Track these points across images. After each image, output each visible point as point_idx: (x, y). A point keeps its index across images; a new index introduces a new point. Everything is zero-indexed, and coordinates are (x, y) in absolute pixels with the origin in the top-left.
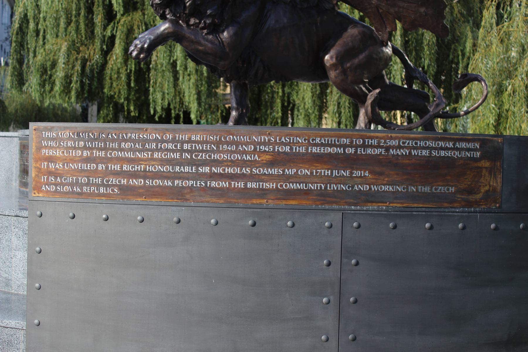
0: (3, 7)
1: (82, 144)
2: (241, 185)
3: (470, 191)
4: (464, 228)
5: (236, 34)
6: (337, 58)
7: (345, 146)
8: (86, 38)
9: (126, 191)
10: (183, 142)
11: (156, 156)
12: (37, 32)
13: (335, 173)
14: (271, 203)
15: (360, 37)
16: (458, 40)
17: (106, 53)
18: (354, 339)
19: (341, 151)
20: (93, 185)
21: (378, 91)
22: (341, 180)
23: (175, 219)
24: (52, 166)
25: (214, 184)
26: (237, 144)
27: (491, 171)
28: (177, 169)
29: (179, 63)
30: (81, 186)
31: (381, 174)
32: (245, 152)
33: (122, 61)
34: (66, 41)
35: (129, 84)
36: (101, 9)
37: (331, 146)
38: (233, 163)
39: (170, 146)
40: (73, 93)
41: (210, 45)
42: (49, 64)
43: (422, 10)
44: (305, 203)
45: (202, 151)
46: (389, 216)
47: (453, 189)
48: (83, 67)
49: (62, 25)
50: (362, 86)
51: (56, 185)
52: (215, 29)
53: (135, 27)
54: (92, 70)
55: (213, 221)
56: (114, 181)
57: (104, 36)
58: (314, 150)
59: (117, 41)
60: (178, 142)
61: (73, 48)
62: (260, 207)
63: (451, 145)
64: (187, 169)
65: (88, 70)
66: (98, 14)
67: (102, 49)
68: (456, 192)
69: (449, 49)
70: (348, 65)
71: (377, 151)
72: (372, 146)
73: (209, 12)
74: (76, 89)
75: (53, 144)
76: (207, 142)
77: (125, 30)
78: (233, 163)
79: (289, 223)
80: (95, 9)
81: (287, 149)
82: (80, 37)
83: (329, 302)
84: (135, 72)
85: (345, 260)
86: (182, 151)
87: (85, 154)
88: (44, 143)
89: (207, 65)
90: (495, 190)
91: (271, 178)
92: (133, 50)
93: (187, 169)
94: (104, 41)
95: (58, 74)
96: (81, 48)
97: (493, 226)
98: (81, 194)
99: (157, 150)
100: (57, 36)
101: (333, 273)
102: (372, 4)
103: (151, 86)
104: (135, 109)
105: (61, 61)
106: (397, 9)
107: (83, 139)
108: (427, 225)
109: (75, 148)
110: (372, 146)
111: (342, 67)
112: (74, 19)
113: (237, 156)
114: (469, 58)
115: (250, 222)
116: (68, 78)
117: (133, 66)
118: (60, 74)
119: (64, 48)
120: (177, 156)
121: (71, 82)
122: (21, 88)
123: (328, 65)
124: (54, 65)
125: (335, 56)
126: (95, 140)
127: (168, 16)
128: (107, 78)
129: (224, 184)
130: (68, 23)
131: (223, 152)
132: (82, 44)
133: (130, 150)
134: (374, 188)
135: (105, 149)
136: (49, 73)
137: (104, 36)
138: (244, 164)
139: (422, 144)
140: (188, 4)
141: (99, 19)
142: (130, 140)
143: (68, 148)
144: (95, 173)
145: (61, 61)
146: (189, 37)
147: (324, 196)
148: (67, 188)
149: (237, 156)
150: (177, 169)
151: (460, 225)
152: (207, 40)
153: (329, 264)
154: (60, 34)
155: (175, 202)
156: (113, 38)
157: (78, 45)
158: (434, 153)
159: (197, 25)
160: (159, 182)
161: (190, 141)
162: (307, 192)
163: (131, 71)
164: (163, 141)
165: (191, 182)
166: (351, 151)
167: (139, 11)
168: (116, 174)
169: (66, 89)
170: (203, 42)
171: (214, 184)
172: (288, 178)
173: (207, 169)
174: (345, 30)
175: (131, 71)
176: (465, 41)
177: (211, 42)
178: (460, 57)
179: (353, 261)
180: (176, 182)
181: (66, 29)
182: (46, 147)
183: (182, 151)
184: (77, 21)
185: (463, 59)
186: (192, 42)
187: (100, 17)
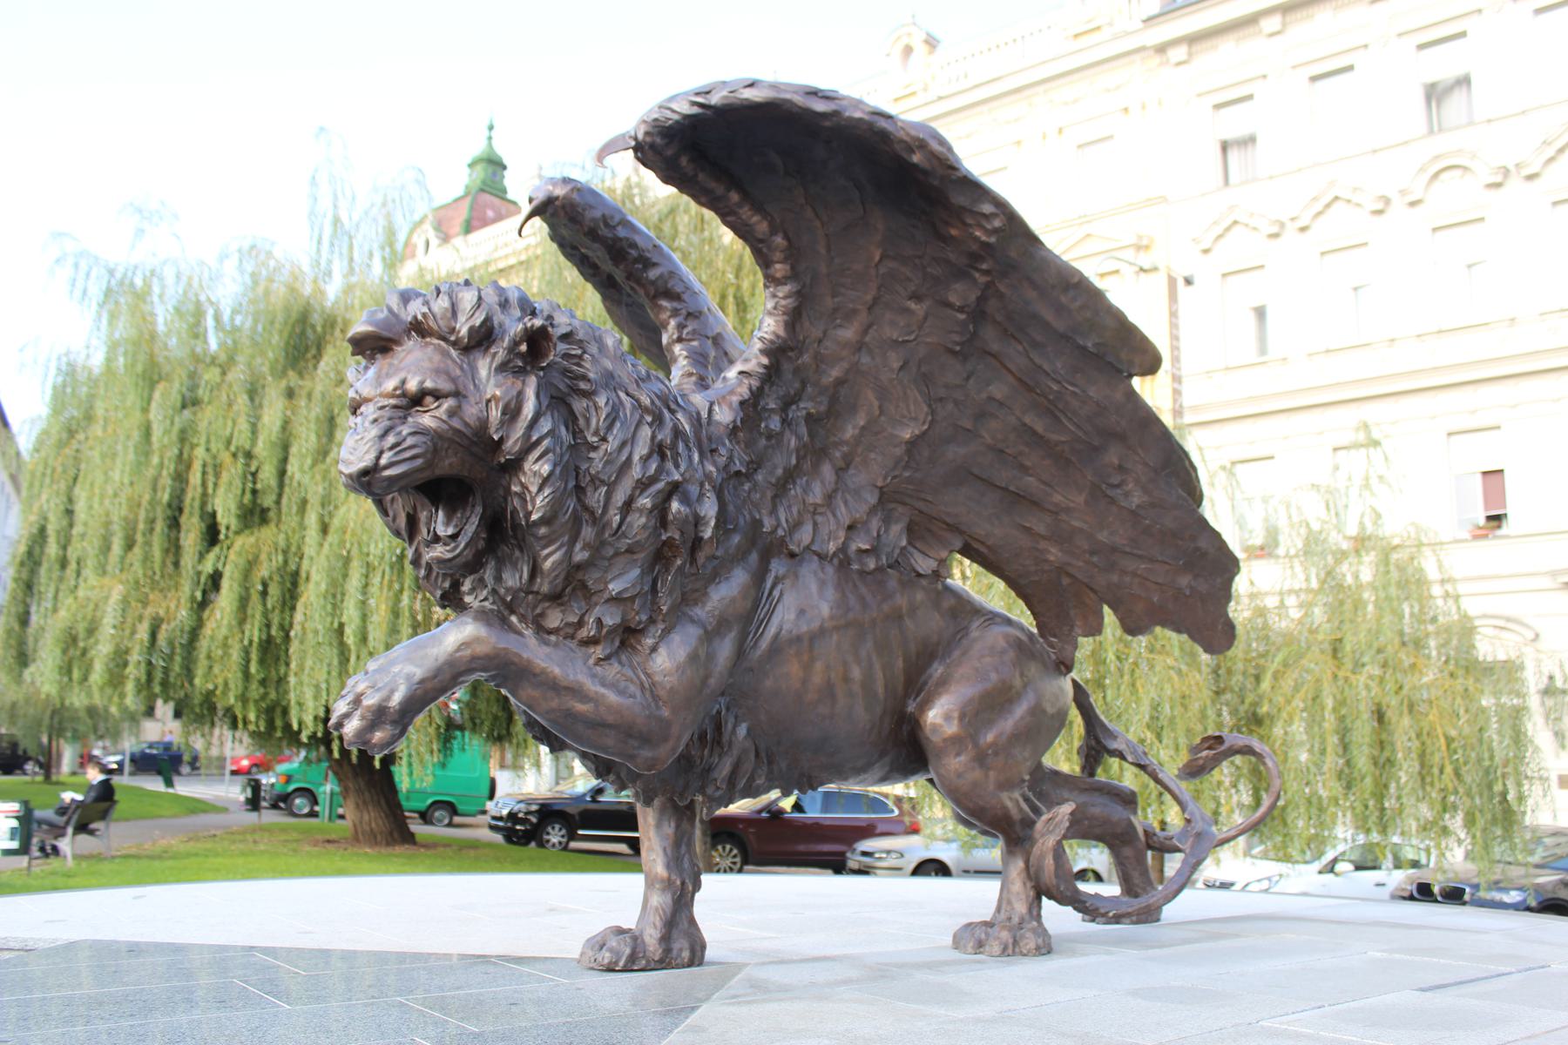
0: (8, 508)
6: (962, 717)
8: (162, 576)
12: (63, 563)
29: (348, 631)
34: (121, 582)
36: (195, 520)
40: (130, 687)
42: (81, 628)
48: (153, 635)
53: (263, 557)
54: (171, 643)
59: (225, 584)
61: (137, 596)
66: (188, 531)
67: (193, 599)
74: (138, 680)
77: (242, 561)
80: (183, 520)
89: (584, 757)
92: (347, 716)
95: (100, 647)
96: (151, 597)
100: (104, 573)
102: (1046, 561)
103: (292, 674)
104: (258, 717)
106: (1115, 578)
111: (976, 745)
112: (139, 538)
116: (120, 659)
117: (256, 633)
118: (102, 650)
119: (116, 596)
121: (126, 664)
122: (20, 675)
124: (91, 631)
125: (956, 715)
127: (468, 599)
128: (202, 656)
130: (129, 545)
136: (81, 644)
140: (548, 564)
141: (191, 536)
145: (107, 629)
146: (544, 671)
154: (109, 568)
156: (216, 579)
159: (570, 631)
163: (251, 642)
167: (272, 525)
169: (115, 679)
175: (251, 642)
181: (123, 559)
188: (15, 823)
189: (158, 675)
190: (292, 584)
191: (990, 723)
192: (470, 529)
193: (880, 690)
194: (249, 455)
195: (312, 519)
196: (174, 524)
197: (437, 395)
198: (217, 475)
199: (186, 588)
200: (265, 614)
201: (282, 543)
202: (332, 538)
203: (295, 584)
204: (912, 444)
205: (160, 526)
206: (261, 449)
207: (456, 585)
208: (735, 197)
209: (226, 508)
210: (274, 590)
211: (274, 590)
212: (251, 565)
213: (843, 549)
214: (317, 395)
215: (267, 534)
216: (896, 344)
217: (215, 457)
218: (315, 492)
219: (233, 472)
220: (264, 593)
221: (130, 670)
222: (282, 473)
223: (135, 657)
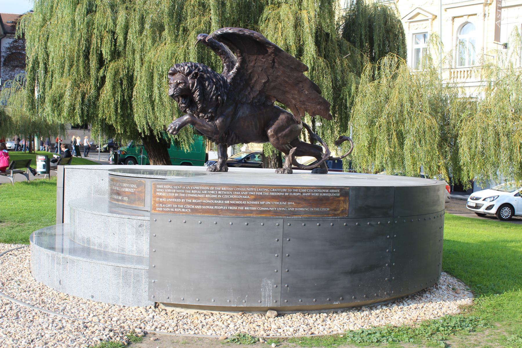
1: (174, 191)
2: (242, 208)
3: (336, 210)
4: (333, 225)
5: (223, 121)
7: (284, 192)
8: (84, 77)
9: (194, 211)
10: (218, 191)
11: (207, 196)
13: (280, 203)
14: (255, 216)
15: (286, 120)
16: (345, 84)
17: (99, 88)
18: (288, 271)
19: (283, 194)
20: (179, 208)
21: (295, 148)
22: (283, 206)
23: (215, 222)
24: (161, 200)
25: (231, 208)
26: (241, 191)
27: (344, 201)
28: (216, 202)
30: (174, 208)
31: (299, 203)
32: (244, 195)
33: (111, 94)
35: (116, 110)
36: (95, 56)
37: (279, 192)
38: (239, 199)
39: (213, 192)
41: (210, 127)
43: (318, 107)
44: (268, 216)
45: (226, 194)
46: (302, 221)
47: (328, 209)
49: (67, 67)
50: (287, 146)
51: (163, 208)
52: (212, 119)
53: (120, 70)
54: (89, 101)
55: (230, 223)
56: (189, 206)
57: (97, 77)
58: (272, 194)
59: (107, 80)
60: (216, 190)
61: (76, 84)
62: (250, 217)
63: (327, 191)
64: (220, 202)
65: (86, 100)
67: (96, 86)
68: (330, 210)
69: (340, 91)
70: (280, 135)
71: (298, 194)
72: (295, 192)
73: (210, 111)
75: (161, 190)
76: (228, 191)
77: (113, 72)
78: (239, 199)
79: (262, 224)
80: (90, 57)
81: (261, 193)
82: (79, 76)
83: (278, 256)
84: (120, 102)
85: (284, 239)
86: (218, 194)
87: (176, 195)
88: (158, 190)
90: (345, 209)
91: (254, 205)
93: (220, 202)
94: (98, 79)
97: (345, 224)
98: (174, 212)
99: (207, 194)
101: (279, 244)
105: (67, 94)
107: (175, 189)
108: (318, 224)
109: (171, 192)
110: (295, 192)
113: (241, 197)
114: (353, 97)
115: (246, 224)
116: (72, 108)
117: (119, 98)
118: (67, 103)
119: (69, 85)
120: (215, 196)
123: (269, 135)
124: (61, 96)
126: (180, 189)
129: (235, 208)
130: (71, 66)
131: (235, 195)
132: (81, 82)
133: (196, 193)
134: (296, 209)
135: (185, 193)
137: (97, 77)
138: (243, 199)
139: (316, 191)
142: (196, 189)
143: (168, 192)
144: (180, 203)
145: (67, 94)
147: (276, 213)
148: (168, 209)
149: (241, 197)
150: (216, 202)
151: (331, 224)
152: (208, 124)
153: (278, 240)
155: (214, 215)
156: (104, 78)
157: (79, 82)
158: (321, 195)
160: (208, 207)
161: (221, 190)
162: (269, 211)
163: (117, 101)
164: (210, 190)
165: (221, 207)
166: (287, 194)
168: (190, 203)
170: (206, 125)
171: (231, 208)
172: (261, 206)
173: (228, 202)
174: (279, 116)
175: (117, 101)
176: (351, 86)
177: (210, 125)
178: (348, 96)
179: (288, 239)
180: (215, 207)
181: (69, 70)
182: (158, 192)
183: (218, 194)
184: (78, 65)
185: (350, 97)
186: (201, 126)
187: (94, 62)
188: (44, 163)
189: (85, 113)
190: (131, 79)
191: (280, 132)
192: (188, 102)
193: (258, 127)
194: (114, 33)
195: (137, 56)
196: (87, 57)
197: (182, 83)
198: (102, 40)
199: (93, 82)
200: (123, 91)
201: (127, 65)
202: (146, 65)
203: (132, 81)
204: (265, 83)
205: (82, 59)
206: (118, 30)
207: (186, 110)
208: (230, 44)
209: (106, 51)
210: (125, 82)
211: (125, 82)
212: (117, 73)
213: (252, 101)
214: (137, 10)
215: (121, 61)
216: (260, 66)
217: (100, 33)
218: (138, 47)
219: (107, 38)
220: (121, 84)
221: (77, 110)
222: (125, 39)
223: (78, 106)
